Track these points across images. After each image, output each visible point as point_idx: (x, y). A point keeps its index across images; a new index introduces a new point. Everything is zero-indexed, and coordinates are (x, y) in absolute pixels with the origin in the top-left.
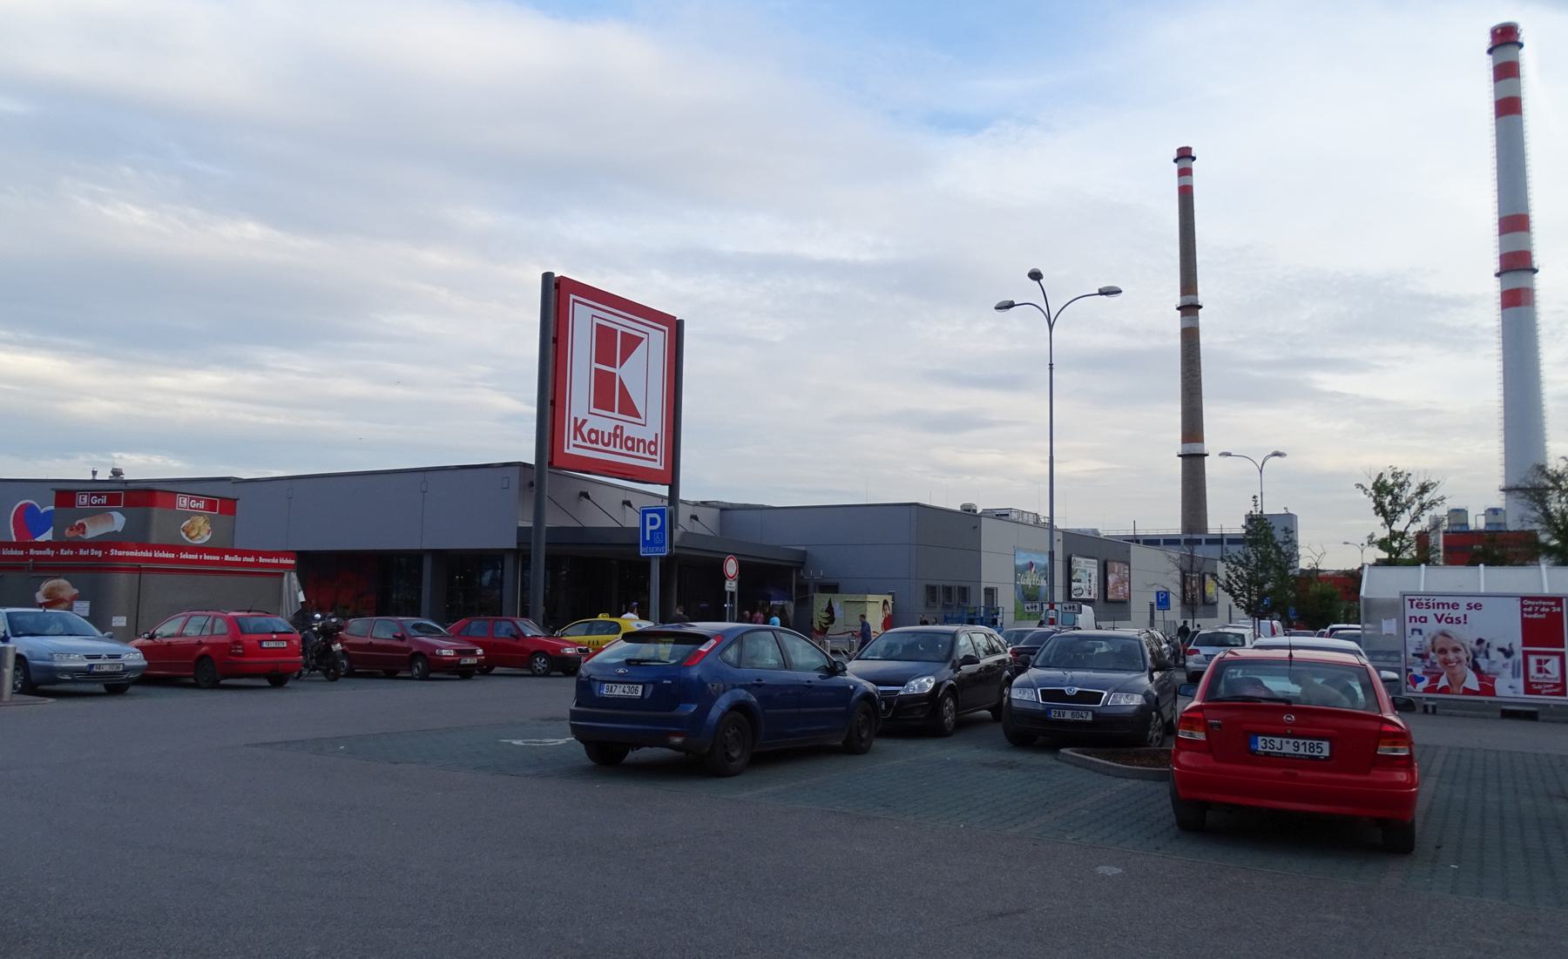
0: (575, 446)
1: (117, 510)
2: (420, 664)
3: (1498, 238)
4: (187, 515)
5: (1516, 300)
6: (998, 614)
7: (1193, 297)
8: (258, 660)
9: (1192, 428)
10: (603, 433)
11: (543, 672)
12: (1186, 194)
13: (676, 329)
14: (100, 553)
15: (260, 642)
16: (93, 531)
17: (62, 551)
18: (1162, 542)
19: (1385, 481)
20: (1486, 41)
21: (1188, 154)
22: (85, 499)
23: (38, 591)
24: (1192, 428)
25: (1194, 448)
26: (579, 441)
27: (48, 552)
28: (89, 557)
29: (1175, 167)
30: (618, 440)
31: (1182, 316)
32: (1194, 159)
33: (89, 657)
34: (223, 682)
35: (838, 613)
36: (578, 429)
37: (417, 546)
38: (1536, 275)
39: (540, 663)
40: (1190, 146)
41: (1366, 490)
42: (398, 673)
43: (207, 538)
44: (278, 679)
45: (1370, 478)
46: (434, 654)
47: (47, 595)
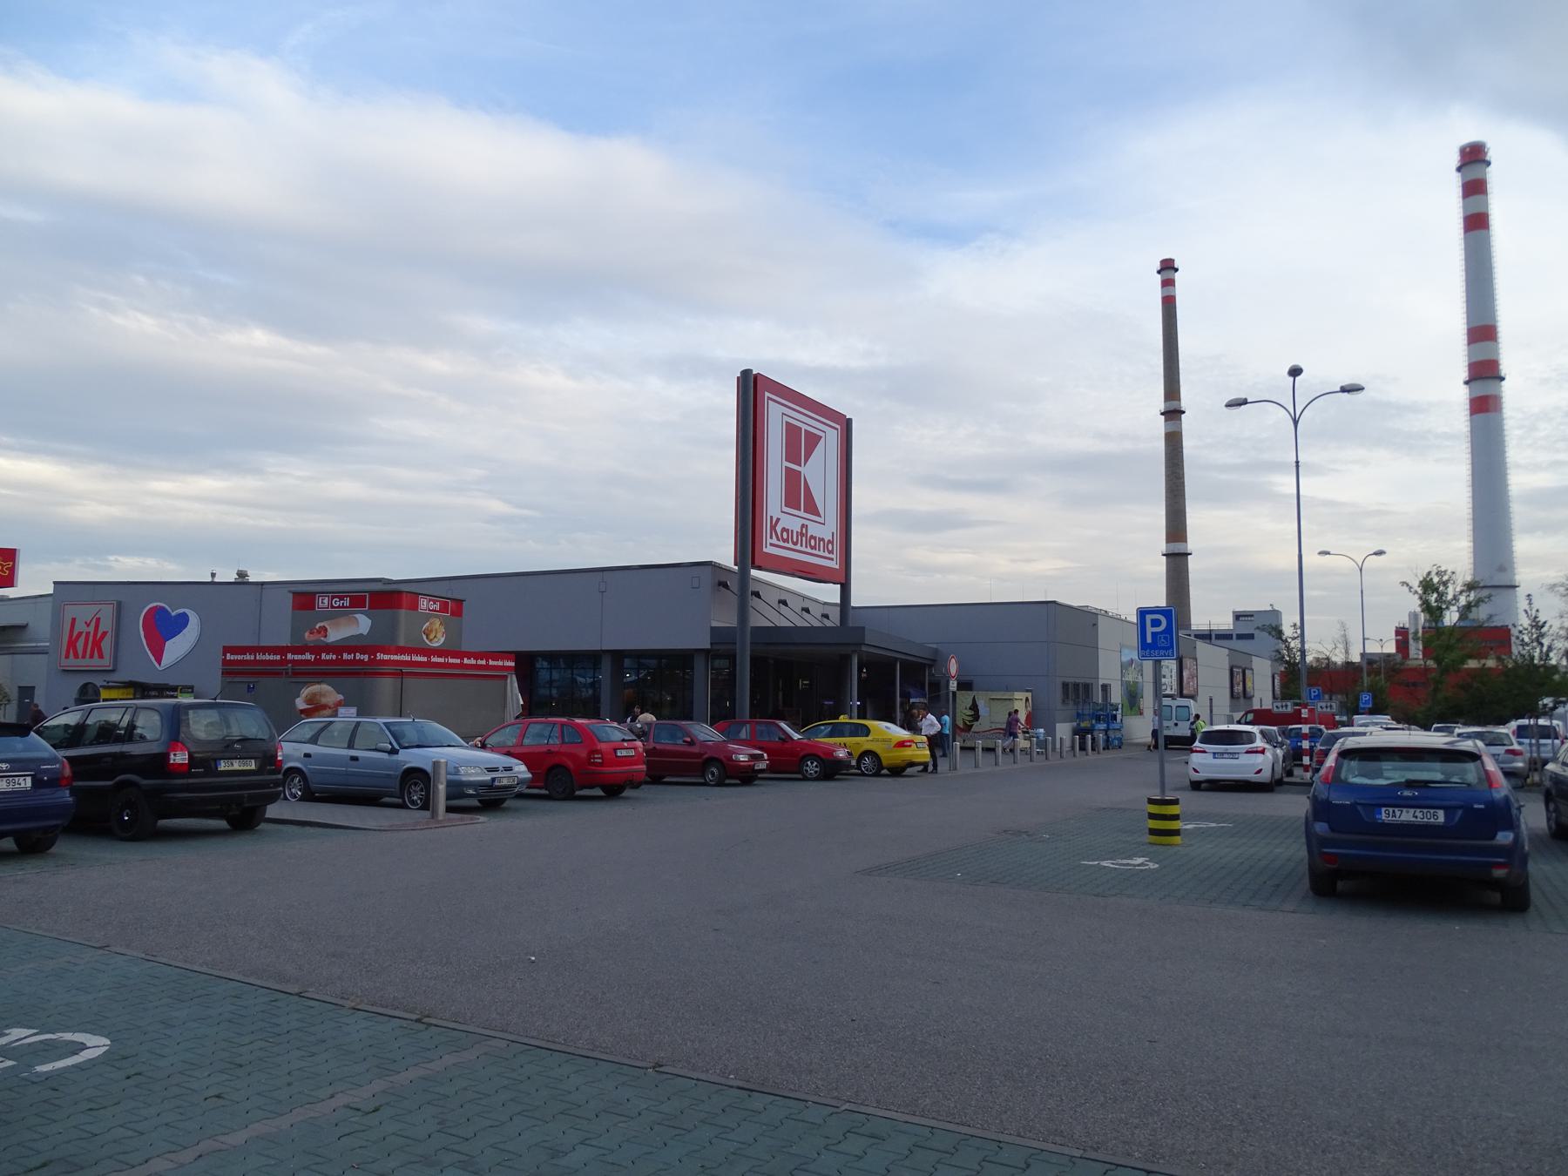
0: (771, 545)
1: (361, 613)
2: (715, 770)
3: (1466, 347)
4: (427, 618)
5: (1484, 406)
6: (1117, 710)
7: (1177, 402)
8: (619, 769)
9: (1176, 528)
10: (792, 531)
11: (815, 776)
12: (1169, 304)
13: (847, 425)
14: (366, 658)
15: (615, 750)
16: (335, 634)
17: (323, 655)
18: (1234, 637)
19: (1431, 579)
20: (1455, 160)
21: (1169, 266)
22: (326, 601)
23: (299, 696)
24: (1176, 528)
25: (1177, 547)
26: (774, 541)
27: (308, 656)
28: (354, 662)
29: (1158, 278)
30: (804, 539)
31: (1166, 420)
32: (1176, 270)
33: (490, 770)
34: (577, 793)
35: (982, 711)
36: (773, 528)
37: (598, 648)
38: (1503, 383)
39: (812, 767)
40: (1172, 257)
41: (1411, 588)
42: (664, 778)
43: (443, 640)
44: (613, 791)
45: (1416, 576)
46: (730, 759)
47: (309, 701)
